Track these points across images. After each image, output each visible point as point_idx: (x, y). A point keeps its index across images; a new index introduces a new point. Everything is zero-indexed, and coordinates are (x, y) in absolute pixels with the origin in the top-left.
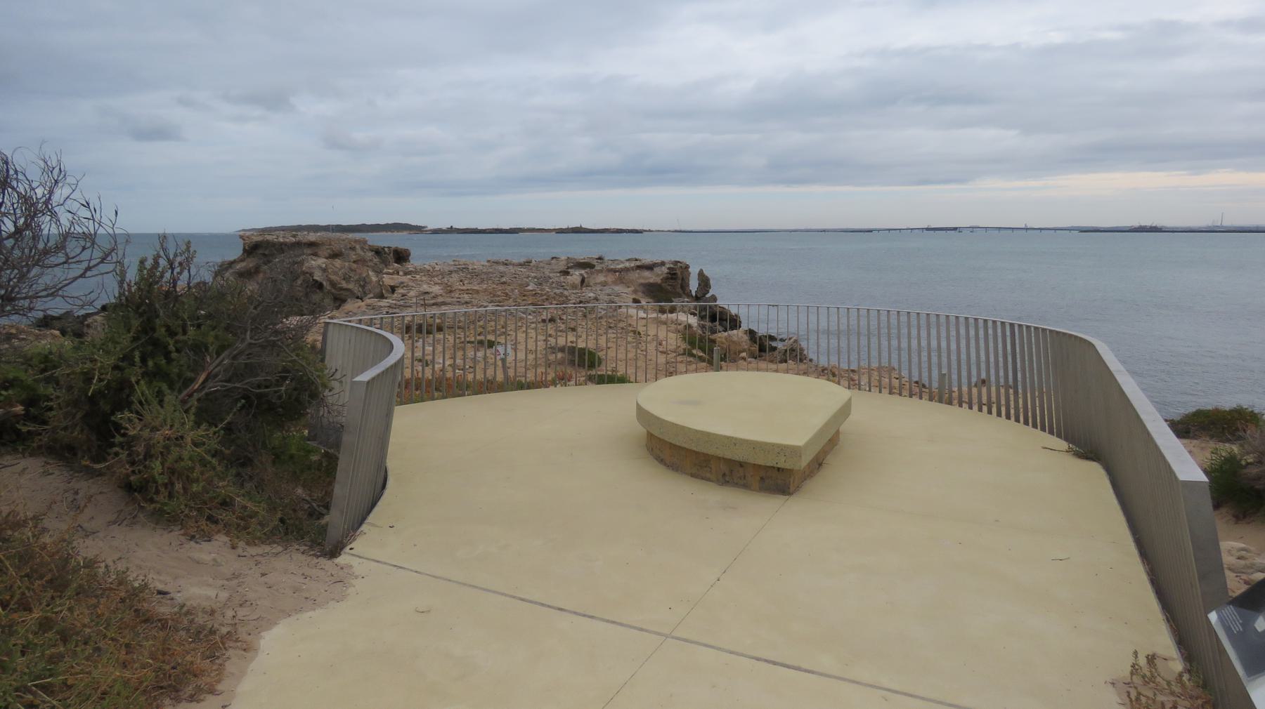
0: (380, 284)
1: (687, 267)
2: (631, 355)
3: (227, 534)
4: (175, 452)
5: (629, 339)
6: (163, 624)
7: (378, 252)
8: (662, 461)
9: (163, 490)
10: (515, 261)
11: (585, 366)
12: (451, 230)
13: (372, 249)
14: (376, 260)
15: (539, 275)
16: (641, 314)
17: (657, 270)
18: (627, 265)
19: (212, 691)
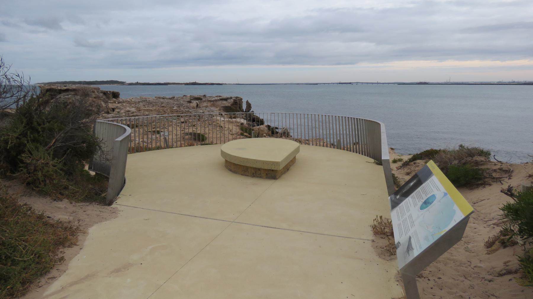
0: (107, 107)
1: (241, 99)
2: (219, 136)
3: (68, 199)
4: (46, 169)
5: (218, 129)
6: (52, 226)
7: (105, 93)
8: (231, 170)
9: (42, 183)
10: (167, 97)
11: (199, 139)
12: (137, 84)
13: (102, 92)
14: (104, 97)
15: (178, 103)
16: (223, 119)
17: (229, 101)
18: (216, 98)
19: (76, 245)
